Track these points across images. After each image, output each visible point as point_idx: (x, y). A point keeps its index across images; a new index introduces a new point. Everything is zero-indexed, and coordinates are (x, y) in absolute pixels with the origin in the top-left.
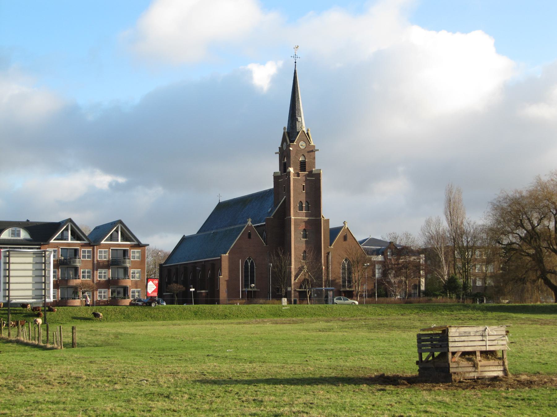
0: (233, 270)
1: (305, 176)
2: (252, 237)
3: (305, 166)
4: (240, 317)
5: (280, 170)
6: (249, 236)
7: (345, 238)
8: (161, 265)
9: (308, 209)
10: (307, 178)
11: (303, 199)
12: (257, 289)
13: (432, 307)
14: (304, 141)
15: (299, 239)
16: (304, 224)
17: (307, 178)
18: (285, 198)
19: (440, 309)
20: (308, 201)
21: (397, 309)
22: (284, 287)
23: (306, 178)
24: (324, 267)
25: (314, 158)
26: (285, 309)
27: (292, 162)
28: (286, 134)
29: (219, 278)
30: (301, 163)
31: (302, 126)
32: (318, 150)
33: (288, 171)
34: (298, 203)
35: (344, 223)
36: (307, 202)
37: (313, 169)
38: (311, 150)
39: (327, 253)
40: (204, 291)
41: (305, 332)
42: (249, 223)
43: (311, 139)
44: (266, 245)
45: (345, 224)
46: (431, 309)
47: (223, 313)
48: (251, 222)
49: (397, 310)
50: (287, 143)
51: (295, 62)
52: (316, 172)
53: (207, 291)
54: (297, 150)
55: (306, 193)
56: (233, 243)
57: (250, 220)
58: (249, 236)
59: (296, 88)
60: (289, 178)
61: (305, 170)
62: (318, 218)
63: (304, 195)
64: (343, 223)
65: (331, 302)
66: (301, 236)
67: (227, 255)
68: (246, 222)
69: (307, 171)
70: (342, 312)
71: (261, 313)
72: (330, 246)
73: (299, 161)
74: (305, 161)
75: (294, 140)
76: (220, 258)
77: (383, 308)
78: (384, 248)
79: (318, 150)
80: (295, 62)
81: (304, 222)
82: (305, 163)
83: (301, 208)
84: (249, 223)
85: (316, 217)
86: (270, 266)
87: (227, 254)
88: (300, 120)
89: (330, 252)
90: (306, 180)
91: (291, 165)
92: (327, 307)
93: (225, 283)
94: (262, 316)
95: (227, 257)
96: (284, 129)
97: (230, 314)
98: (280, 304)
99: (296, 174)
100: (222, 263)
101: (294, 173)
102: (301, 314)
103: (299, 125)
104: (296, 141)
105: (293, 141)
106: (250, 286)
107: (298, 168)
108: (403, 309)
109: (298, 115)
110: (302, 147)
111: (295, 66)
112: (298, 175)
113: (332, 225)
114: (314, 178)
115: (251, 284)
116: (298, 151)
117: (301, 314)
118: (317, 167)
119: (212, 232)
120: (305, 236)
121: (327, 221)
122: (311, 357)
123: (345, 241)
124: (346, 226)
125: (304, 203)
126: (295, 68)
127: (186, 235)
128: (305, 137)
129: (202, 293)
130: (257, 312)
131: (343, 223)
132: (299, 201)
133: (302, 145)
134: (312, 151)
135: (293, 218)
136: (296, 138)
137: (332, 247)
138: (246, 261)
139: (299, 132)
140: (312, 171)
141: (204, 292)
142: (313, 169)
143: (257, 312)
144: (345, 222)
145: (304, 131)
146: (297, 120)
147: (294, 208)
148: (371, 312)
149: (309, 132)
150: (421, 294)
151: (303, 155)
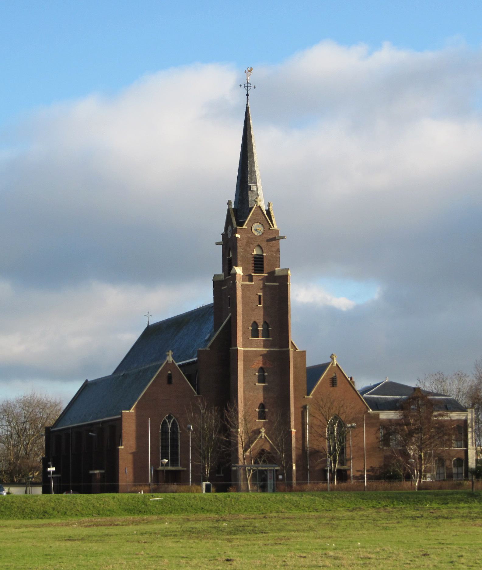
0: (141, 436)
1: (262, 279)
2: (173, 380)
3: (263, 265)
4: (70, 514)
5: (223, 271)
6: (170, 379)
7: (333, 382)
8: (48, 429)
9: (266, 334)
10: (266, 284)
11: (260, 319)
12: (183, 467)
13: (415, 496)
14: (260, 223)
15: (252, 384)
16: (261, 358)
17: (266, 284)
18: (230, 317)
19: (427, 500)
20: (267, 321)
21: (353, 499)
22: (208, 464)
23: (264, 284)
24: (294, 430)
25: (278, 251)
26: (154, 501)
27: (239, 257)
28: (232, 212)
29: (118, 449)
30: (255, 260)
31: (257, 198)
32: (283, 238)
33: (232, 272)
34: (251, 325)
35: (332, 357)
36: (265, 322)
37: (276, 269)
38: (271, 236)
39: (302, 407)
40: (97, 472)
41: (405, 528)
42: (170, 359)
43: (274, 220)
44: (198, 393)
45: (333, 359)
46: (412, 500)
47: (42, 509)
48: (173, 356)
49: (352, 502)
50: (232, 227)
51: (247, 95)
52: (281, 274)
53: (103, 471)
54: (249, 237)
55: (264, 307)
56: (142, 392)
57: (170, 353)
58: (170, 379)
59: (248, 137)
60: (235, 284)
61: (263, 271)
62: (284, 349)
63: (262, 312)
64: (331, 357)
65: (271, 488)
66: (256, 379)
67: (131, 411)
68: (165, 357)
69: (265, 271)
70: (253, 505)
71: (109, 508)
72: (308, 395)
73: (251, 256)
74: (263, 255)
75: (244, 222)
76: (120, 416)
77: (328, 498)
78: (404, 399)
79: (283, 238)
80: (247, 95)
81: (261, 355)
82: (263, 258)
83: (255, 334)
84: (170, 359)
85: (280, 347)
86: (189, 428)
87: (132, 411)
88: (255, 189)
89: (307, 405)
90: (265, 287)
91: (239, 262)
92: (229, 496)
93: (130, 457)
94: (108, 513)
95: (134, 415)
96: (229, 203)
97: (54, 509)
98: (199, 492)
99: (248, 277)
100: (124, 424)
101: (243, 276)
102: (179, 510)
103: (252, 197)
104: (246, 222)
105: (241, 224)
106: (161, 463)
107: (251, 266)
108: (362, 501)
109: (252, 179)
110: (256, 233)
111: (247, 101)
112: (251, 279)
113: (310, 363)
114: (278, 284)
115: (162, 459)
116: (250, 239)
117: (179, 510)
118: (283, 266)
119: (122, 374)
120: (262, 379)
121: (303, 354)
122: (462, 556)
123: (333, 386)
124: (335, 362)
125: (261, 325)
126: (247, 104)
127: (89, 380)
128: (261, 217)
129: (96, 474)
130: (102, 506)
131: (331, 357)
132: (252, 322)
133: (256, 230)
134: (274, 239)
135: (240, 349)
136: (246, 218)
137: (310, 397)
138: (165, 421)
139: (252, 208)
140: (274, 272)
141: (98, 473)
142: (276, 269)
143: (102, 506)
144: (332, 355)
145: (260, 207)
146: (249, 188)
147: (244, 333)
148: (303, 506)
149: (270, 208)
150: (469, 474)
151: (259, 246)
